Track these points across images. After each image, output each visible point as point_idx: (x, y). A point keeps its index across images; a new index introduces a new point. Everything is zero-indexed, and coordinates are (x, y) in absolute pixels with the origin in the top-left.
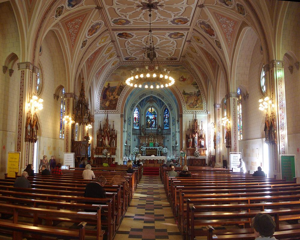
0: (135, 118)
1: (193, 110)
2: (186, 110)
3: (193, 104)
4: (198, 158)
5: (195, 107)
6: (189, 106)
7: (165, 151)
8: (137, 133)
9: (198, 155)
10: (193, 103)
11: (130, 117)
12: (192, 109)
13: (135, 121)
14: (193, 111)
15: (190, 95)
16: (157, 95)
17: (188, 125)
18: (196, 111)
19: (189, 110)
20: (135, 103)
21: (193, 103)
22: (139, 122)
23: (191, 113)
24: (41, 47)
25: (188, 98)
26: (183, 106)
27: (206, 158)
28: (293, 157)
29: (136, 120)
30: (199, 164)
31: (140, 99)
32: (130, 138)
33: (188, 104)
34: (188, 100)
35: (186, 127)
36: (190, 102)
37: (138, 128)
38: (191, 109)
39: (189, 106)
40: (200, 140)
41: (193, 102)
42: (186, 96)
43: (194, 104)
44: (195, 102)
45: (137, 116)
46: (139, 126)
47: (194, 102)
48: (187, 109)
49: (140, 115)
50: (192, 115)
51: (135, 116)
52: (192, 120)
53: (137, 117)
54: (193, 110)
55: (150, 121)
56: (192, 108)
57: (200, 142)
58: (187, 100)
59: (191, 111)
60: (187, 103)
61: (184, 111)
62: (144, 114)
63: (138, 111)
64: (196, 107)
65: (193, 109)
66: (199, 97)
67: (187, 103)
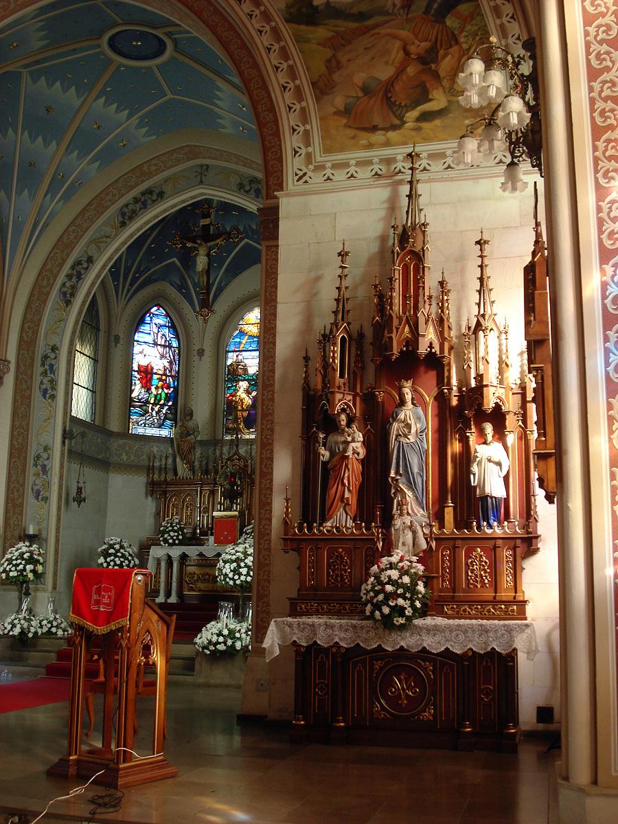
0: (146, 373)
1: (387, 152)
2: (319, 158)
3: (387, 91)
4: (408, 641)
5: (412, 115)
6: (347, 111)
7: (235, 571)
8: (157, 464)
9: (400, 611)
10: (389, 85)
11: (54, 349)
12: (378, 137)
13: (147, 385)
14: (389, 161)
15: (361, 16)
16: (241, 186)
17: (327, 296)
18: (423, 149)
19: (341, 150)
20: (92, 251)
21: (391, 82)
22: (174, 397)
23: (364, 174)
24: (306, 349)
25: (338, 43)
26: (288, 120)
27: (520, 643)
28: (173, 643)
29: (155, 382)
30: (427, 715)
31: (123, 224)
32: (48, 485)
33: (339, 101)
34: (339, 66)
35: (309, 316)
36: (360, 78)
37: (165, 433)
38: (364, 138)
39: (347, 111)
40: (465, 441)
41: (384, 73)
42: (321, 32)
43: (397, 87)
44: (411, 70)
45: (162, 356)
46: (175, 420)
47: (401, 71)
48: (327, 150)
49: (185, 355)
50: (381, 194)
51: (139, 360)
52: (375, 247)
53: (159, 365)
54: (388, 144)
55: (248, 392)
56: (374, 129)
57: (466, 459)
58: (333, 65)
59: (368, 163)
60: (322, 89)
61: (292, 165)
62: (208, 346)
63: (173, 327)
64: (426, 117)
65: (391, 135)
66: (451, 22)
67: (322, 89)
